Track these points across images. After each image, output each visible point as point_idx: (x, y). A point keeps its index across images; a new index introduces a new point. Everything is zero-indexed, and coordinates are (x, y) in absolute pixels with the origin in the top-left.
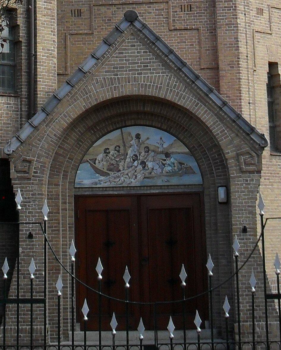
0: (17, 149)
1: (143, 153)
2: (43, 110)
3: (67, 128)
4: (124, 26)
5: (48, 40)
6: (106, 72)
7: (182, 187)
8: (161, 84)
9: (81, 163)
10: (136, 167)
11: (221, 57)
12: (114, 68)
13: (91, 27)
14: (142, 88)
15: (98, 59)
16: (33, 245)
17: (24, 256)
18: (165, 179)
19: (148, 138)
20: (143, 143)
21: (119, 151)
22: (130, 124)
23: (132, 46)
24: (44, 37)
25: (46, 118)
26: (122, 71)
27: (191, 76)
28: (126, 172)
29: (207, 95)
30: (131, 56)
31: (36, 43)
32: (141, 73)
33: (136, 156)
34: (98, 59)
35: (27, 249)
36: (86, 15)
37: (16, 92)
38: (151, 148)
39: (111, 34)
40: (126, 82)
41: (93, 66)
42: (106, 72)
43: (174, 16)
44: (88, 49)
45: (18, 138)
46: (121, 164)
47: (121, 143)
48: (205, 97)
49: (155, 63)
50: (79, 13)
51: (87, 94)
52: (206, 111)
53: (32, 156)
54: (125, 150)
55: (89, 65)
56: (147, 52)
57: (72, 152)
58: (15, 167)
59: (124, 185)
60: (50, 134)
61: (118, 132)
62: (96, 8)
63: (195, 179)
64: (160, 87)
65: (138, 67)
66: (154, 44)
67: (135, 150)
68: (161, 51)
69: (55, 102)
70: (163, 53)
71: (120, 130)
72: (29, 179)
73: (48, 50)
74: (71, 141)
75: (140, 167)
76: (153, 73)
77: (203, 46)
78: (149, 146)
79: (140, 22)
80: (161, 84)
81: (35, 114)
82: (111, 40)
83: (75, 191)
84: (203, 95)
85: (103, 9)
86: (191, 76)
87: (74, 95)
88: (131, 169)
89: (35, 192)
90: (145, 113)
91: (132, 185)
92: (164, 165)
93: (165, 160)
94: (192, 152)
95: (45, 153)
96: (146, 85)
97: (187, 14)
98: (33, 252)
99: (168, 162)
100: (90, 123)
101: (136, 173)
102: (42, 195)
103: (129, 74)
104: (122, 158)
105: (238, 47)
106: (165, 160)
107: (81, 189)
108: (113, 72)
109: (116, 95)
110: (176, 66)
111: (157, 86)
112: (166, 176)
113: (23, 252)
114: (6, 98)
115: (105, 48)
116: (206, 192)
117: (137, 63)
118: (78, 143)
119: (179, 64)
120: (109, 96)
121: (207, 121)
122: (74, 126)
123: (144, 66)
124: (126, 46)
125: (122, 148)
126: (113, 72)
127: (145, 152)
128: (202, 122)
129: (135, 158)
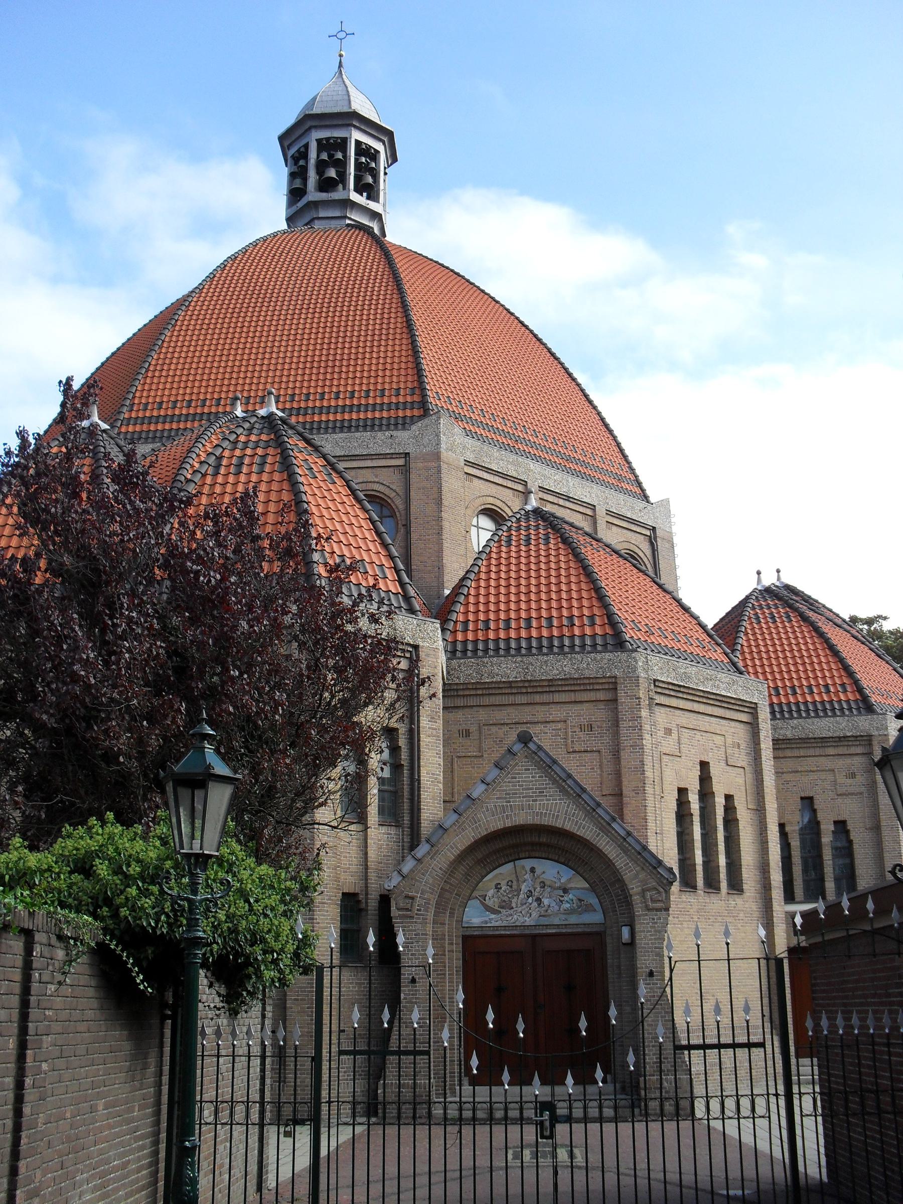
0: (399, 884)
2: (428, 841)
4: (517, 747)
11: (625, 782)
13: (480, 749)
15: (488, 784)
17: (406, 1003)
18: (563, 917)
19: (544, 872)
20: (539, 877)
21: (511, 887)
27: (592, 804)
28: (520, 909)
29: (610, 825)
31: (419, 767)
32: (536, 800)
33: (530, 891)
34: (488, 784)
35: (409, 995)
36: (475, 735)
37: (397, 821)
38: (548, 883)
39: (503, 757)
43: (572, 737)
45: (399, 872)
46: (514, 901)
47: (513, 878)
48: (608, 827)
50: (468, 733)
54: (519, 886)
55: (478, 791)
59: (518, 924)
61: (511, 865)
62: (486, 728)
63: (596, 917)
64: (558, 816)
68: (558, 775)
69: (440, 832)
70: (561, 778)
72: (412, 917)
73: (433, 774)
79: (535, 743)
81: (418, 845)
82: (503, 763)
84: (605, 824)
85: (494, 729)
86: (592, 804)
91: (526, 924)
92: (561, 901)
94: (593, 888)
99: (566, 898)
100: (479, 855)
102: (426, 935)
103: (522, 801)
108: (505, 798)
109: (508, 824)
110: (575, 792)
113: (405, 999)
115: (496, 772)
116: (608, 932)
117: (532, 789)
119: (578, 790)
120: (500, 825)
125: (515, 883)
126: (505, 798)
129: (530, 894)
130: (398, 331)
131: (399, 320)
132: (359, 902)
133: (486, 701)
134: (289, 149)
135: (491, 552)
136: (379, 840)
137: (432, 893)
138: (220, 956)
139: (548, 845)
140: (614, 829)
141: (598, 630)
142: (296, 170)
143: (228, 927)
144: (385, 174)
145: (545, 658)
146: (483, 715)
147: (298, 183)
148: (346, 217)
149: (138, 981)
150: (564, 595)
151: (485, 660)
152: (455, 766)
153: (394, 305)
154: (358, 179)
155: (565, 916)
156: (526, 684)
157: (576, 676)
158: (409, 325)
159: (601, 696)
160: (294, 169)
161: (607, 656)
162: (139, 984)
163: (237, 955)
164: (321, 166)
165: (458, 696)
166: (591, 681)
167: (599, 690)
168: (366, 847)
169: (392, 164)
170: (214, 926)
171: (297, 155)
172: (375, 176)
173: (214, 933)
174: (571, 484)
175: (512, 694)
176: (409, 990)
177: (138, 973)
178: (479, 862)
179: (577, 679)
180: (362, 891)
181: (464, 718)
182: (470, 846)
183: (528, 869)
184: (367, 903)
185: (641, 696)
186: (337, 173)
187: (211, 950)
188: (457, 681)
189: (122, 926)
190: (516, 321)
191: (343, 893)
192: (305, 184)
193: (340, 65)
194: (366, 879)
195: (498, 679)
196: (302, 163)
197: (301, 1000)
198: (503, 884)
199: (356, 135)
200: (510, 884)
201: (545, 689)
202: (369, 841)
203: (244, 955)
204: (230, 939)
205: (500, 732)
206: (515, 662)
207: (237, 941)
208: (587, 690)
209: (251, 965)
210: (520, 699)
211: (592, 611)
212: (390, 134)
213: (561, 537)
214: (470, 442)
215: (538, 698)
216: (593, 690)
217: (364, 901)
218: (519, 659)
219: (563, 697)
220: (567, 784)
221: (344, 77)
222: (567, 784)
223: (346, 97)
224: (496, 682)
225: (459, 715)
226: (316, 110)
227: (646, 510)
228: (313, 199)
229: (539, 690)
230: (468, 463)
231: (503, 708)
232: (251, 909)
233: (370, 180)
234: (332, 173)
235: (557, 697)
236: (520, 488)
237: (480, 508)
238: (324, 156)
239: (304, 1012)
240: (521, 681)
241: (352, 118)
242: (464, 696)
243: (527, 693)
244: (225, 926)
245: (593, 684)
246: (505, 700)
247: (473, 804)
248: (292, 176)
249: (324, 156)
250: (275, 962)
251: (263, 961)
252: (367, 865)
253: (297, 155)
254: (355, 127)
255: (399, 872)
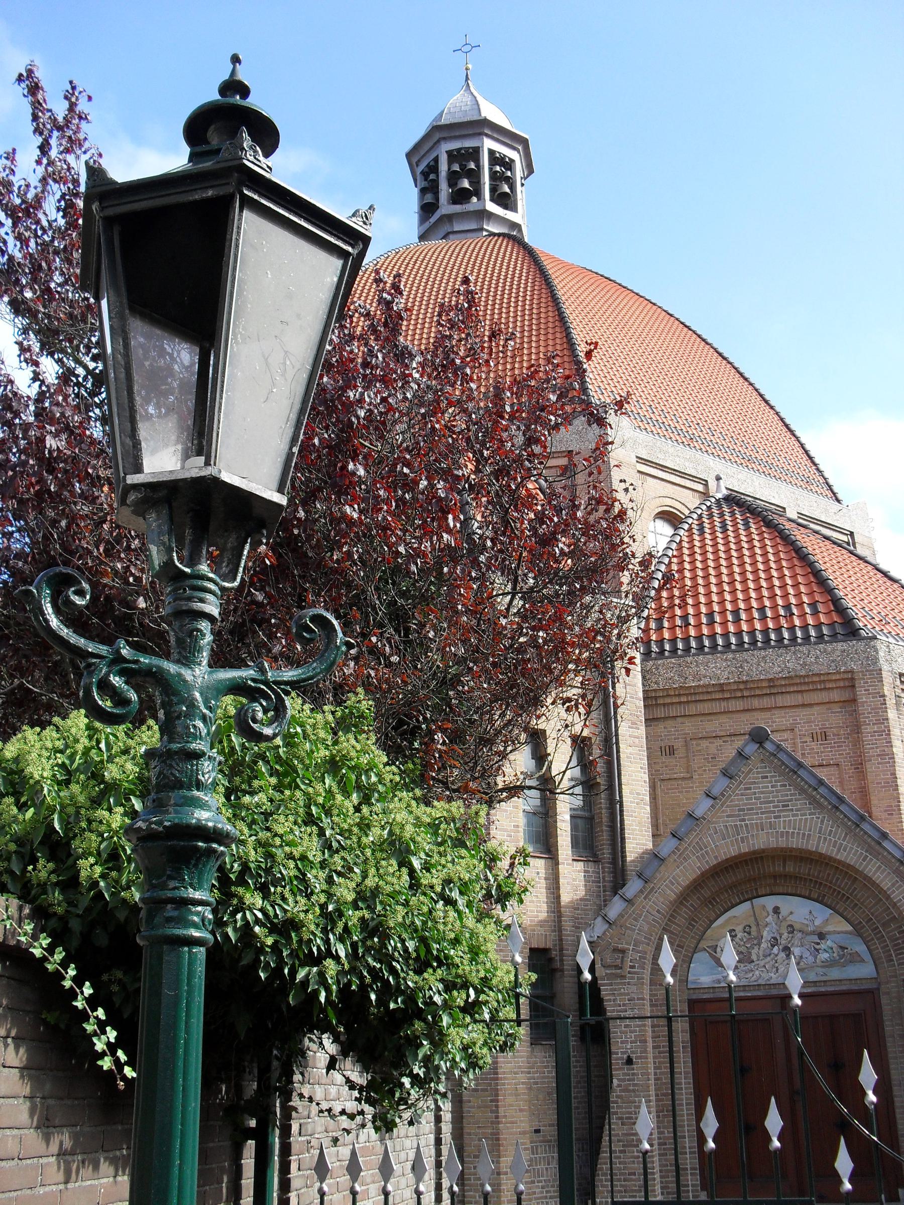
0: (604, 933)
1: (786, 934)
2: (640, 875)
3: (675, 901)
4: (751, 749)
5: (638, 781)
6: (728, 816)
7: (845, 982)
8: (810, 830)
9: (694, 952)
10: (777, 955)
11: (874, 801)
12: (740, 810)
13: (688, 769)
14: (782, 837)
15: (715, 799)
16: (633, 1074)
17: (621, 1091)
18: (820, 971)
19: (791, 913)
20: (785, 919)
21: (749, 933)
22: (764, 893)
23: (763, 777)
24: (630, 775)
25: (644, 887)
26: (751, 814)
27: (853, 817)
28: (762, 963)
29: (880, 844)
30: (762, 793)
31: (620, 784)
32: (779, 817)
33: (775, 938)
34: (715, 799)
35: (624, 1080)
36: (680, 752)
37: (595, 855)
38: (797, 926)
39: (732, 762)
40: (758, 830)
41: (709, 810)
42: (728, 816)
43: (803, 748)
44: (687, 799)
45: (605, 918)
46: (754, 952)
47: (751, 921)
48: (877, 847)
49: (799, 800)
50: (671, 751)
51: (701, 849)
52: (880, 867)
53: (627, 944)
54: (759, 931)
55: (702, 807)
56: (785, 786)
57: (683, 937)
58: (602, 960)
59: (761, 982)
60: (651, 910)
61: (747, 904)
62: (694, 742)
63: (865, 970)
64: (809, 835)
65: (774, 807)
66: (795, 773)
67: (774, 931)
68: (806, 783)
69: (656, 863)
70: (810, 786)
71: (749, 903)
72: (623, 977)
73: (638, 794)
74: (680, 920)
75: (783, 955)
76: (797, 815)
77: (846, 787)
78: (793, 924)
79: (773, 742)
80: (810, 830)
81: (624, 885)
82: (732, 770)
83: (689, 995)
84: (873, 843)
85: (704, 744)
86: (853, 817)
87: (683, 852)
88: (769, 959)
89: (633, 995)
90: (786, 876)
91: (772, 982)
92: (817, 950)
93: (818, 944)
94: (858, 930)
95: (645, 938)
96: (787, 832)
97: (821, 744)
98: (634, 1085)
99: (823, 946)
100: (706, 893)
101: (777, 965)
102: (643, 999)
103: (761, 818)
104: (755, 942)
105: (897, 785)
106: (818, 944)
107: (697, 991)
108: (739, 816)
109: (745, 849)
110: (830, 803)
111: (804, 834)
112: (822, 967)
113: (619, 1086)
114: (582, 863)
115: (725, 782)
116: (883, 988)
117: (773, 802)
118: (690, 924)
119: (834, 801)
120: (733, 851)
121: (882, 881)
122: (685, 899)
123: (783, 806)
124: (754, 778)
125: (754, 929)
126: (739, 816)
127: (789, 933)
128: (874, 882)
129: (775, 942)
130: (550, 325)
131: (550, 314)
132: (551, 960)
133: (693, 709)
134: (417, 166)
135: (681, 541)
136: (574, 880)
137: (648, 944)
138: (345, 990)
139: (795, 878)
140: (884, 848)
141: (823, 618)
142: (427, 185)
143: (362, 919)
144: (522, 185)
145: (763, 653)
146: (688, 727)
147: (429, 198)
148: (482, 229)
149: (100, 1046)
150: (765, 593)
151: (689, 659)
152: (659, 791)
153: (543, 300)
154: (493, 190)
155: (824, 970)
156: (742, 686)
157: (803, 673)
158: (561, 318)
159: (836, 696)
160: (424, 184)
161: (840, 646)
162: (102, 1055)
163: (387, 992)
164: (453, 178)
165: (657, 705)
166: (822, 678)
167: (832, 688)
168: (558, 888)
169: (528, 176)
170: (324, 914)
171: (427, 170)
172: (512, 187)
173: (325, 931)
174: (757, 484)
175: (724, 699)
176: (624, 1074)
177: (102, 1025)
178: (710, 902)
179: (804, 677)
180: (555, 945)
181: (670, 731)
182: (695, 881)
183: (770, 909)
184: (562, 960)
185: (886, 693)
186: (471, 183)
187: (322, 975)
188: (655, 687)
189: (85, 901)
190: (677, 322)
191: (531, 949)
192: (437, 199)
193: (467, 78)
194: (560, 931)
195: (706, 681)
196: (432, 176)
197: (483, 1090)
198: (739, 929)
199: (489, 144)
200: (747, 929)
201: (764, 692)
202: (561, 881)
203: (402, 993)
204: (368, 950)
205: (712, 747)
206: (726, 660)
207: (386, 959)
208: (817, 689)
209: (419, 1015)
210: (734, 705)
211: (814, 598)
212: (525, 142)
213: (763, 520)
214: (642, 436)
215: (756, 703)
216: (825, 689)
217: (558, 958)
218: (730, 656)
219: (788, 700)
220: (819, 793)
221: (472, 89)
222: (819, 793)
223: (476, 107)
224: (703, 686)
225: (660, 728)
226: (443, 121)
227: (841, 513)
228: (447, 213)
229: (758, 692)
230: (641, 460)
231: (713, 717)
232: (415, 885)
233: (506, 189)
234: (466, 184)
235: (780, 701)
236: (700, 488)
237: (660, 509)
238: (456, 167)
239: (486, 1107)
240: (735, 682)
241: (482, 126)
242: (664, 705)
243: (743, 697)
244: (353, 917)
245: (824, 681)
246: (716, 707)
247: (697, 825)
248: (423, 191)
249: (456, 167)
250: (471, 1008)
251: (446, 1005)
252: (559, 912)
253: (427, 170)
254: (487, 136)
255: (605, 918)
